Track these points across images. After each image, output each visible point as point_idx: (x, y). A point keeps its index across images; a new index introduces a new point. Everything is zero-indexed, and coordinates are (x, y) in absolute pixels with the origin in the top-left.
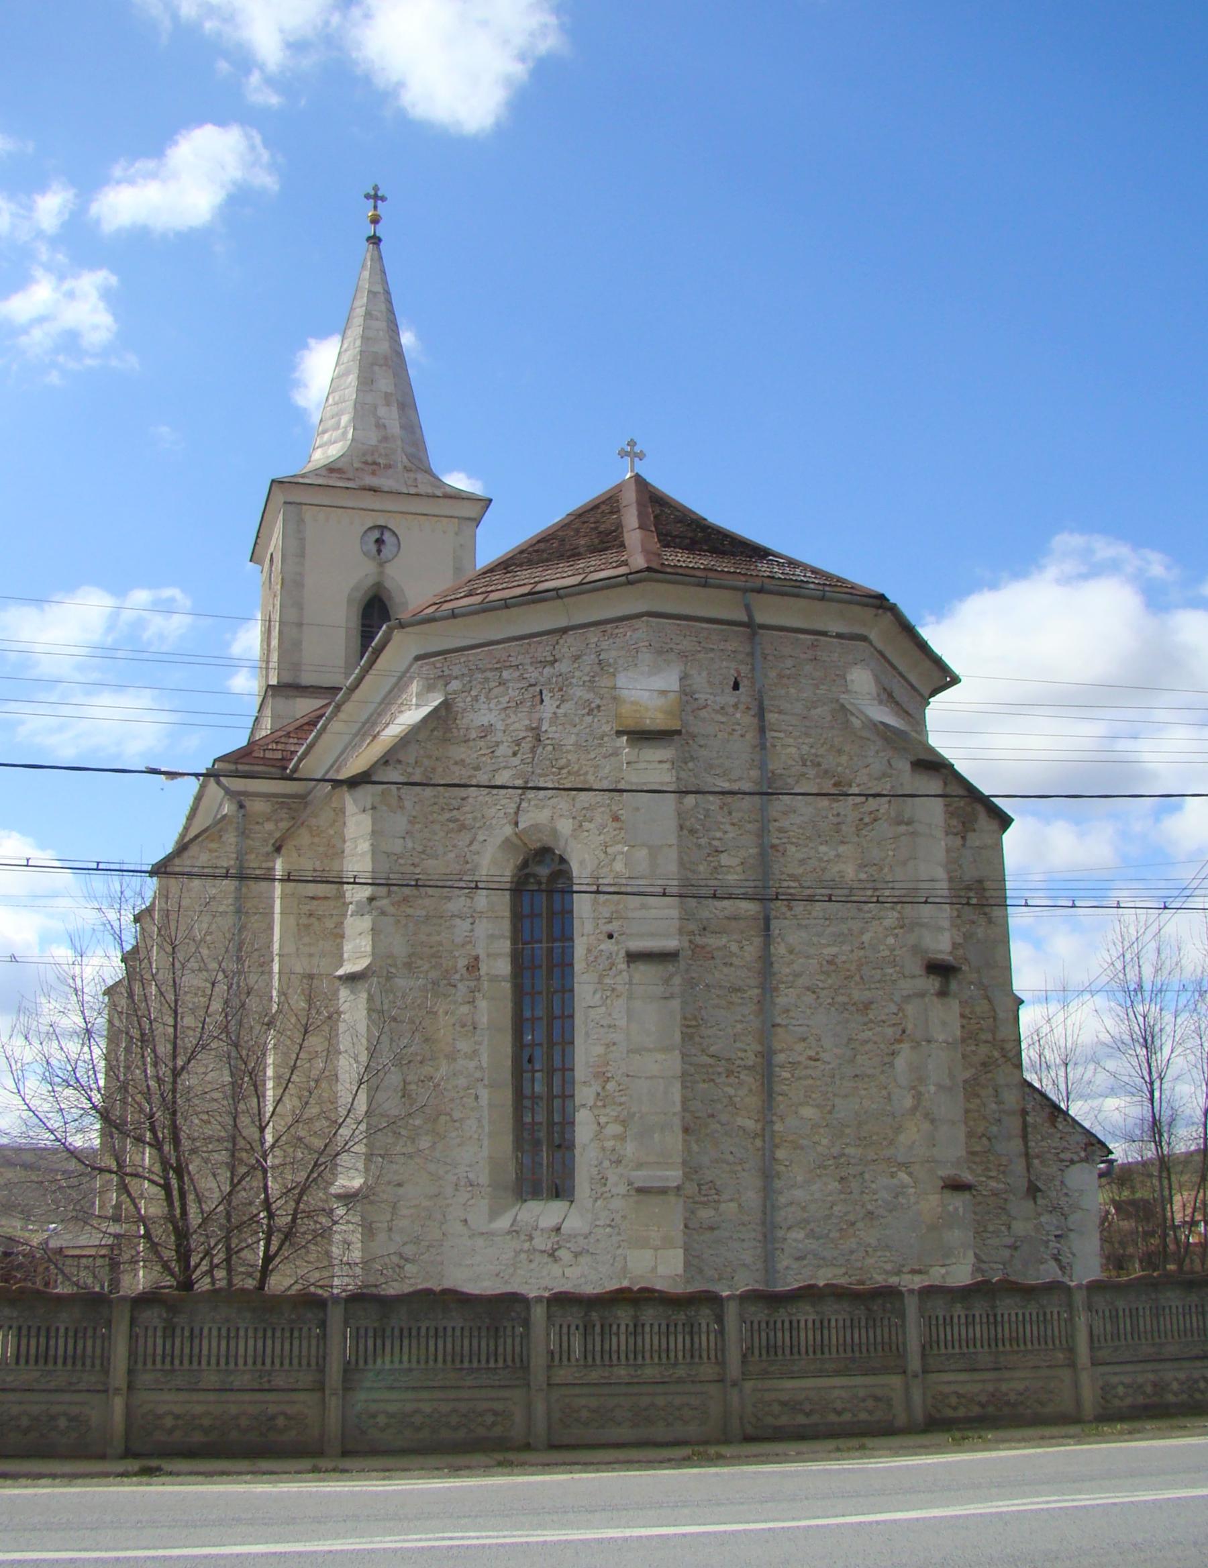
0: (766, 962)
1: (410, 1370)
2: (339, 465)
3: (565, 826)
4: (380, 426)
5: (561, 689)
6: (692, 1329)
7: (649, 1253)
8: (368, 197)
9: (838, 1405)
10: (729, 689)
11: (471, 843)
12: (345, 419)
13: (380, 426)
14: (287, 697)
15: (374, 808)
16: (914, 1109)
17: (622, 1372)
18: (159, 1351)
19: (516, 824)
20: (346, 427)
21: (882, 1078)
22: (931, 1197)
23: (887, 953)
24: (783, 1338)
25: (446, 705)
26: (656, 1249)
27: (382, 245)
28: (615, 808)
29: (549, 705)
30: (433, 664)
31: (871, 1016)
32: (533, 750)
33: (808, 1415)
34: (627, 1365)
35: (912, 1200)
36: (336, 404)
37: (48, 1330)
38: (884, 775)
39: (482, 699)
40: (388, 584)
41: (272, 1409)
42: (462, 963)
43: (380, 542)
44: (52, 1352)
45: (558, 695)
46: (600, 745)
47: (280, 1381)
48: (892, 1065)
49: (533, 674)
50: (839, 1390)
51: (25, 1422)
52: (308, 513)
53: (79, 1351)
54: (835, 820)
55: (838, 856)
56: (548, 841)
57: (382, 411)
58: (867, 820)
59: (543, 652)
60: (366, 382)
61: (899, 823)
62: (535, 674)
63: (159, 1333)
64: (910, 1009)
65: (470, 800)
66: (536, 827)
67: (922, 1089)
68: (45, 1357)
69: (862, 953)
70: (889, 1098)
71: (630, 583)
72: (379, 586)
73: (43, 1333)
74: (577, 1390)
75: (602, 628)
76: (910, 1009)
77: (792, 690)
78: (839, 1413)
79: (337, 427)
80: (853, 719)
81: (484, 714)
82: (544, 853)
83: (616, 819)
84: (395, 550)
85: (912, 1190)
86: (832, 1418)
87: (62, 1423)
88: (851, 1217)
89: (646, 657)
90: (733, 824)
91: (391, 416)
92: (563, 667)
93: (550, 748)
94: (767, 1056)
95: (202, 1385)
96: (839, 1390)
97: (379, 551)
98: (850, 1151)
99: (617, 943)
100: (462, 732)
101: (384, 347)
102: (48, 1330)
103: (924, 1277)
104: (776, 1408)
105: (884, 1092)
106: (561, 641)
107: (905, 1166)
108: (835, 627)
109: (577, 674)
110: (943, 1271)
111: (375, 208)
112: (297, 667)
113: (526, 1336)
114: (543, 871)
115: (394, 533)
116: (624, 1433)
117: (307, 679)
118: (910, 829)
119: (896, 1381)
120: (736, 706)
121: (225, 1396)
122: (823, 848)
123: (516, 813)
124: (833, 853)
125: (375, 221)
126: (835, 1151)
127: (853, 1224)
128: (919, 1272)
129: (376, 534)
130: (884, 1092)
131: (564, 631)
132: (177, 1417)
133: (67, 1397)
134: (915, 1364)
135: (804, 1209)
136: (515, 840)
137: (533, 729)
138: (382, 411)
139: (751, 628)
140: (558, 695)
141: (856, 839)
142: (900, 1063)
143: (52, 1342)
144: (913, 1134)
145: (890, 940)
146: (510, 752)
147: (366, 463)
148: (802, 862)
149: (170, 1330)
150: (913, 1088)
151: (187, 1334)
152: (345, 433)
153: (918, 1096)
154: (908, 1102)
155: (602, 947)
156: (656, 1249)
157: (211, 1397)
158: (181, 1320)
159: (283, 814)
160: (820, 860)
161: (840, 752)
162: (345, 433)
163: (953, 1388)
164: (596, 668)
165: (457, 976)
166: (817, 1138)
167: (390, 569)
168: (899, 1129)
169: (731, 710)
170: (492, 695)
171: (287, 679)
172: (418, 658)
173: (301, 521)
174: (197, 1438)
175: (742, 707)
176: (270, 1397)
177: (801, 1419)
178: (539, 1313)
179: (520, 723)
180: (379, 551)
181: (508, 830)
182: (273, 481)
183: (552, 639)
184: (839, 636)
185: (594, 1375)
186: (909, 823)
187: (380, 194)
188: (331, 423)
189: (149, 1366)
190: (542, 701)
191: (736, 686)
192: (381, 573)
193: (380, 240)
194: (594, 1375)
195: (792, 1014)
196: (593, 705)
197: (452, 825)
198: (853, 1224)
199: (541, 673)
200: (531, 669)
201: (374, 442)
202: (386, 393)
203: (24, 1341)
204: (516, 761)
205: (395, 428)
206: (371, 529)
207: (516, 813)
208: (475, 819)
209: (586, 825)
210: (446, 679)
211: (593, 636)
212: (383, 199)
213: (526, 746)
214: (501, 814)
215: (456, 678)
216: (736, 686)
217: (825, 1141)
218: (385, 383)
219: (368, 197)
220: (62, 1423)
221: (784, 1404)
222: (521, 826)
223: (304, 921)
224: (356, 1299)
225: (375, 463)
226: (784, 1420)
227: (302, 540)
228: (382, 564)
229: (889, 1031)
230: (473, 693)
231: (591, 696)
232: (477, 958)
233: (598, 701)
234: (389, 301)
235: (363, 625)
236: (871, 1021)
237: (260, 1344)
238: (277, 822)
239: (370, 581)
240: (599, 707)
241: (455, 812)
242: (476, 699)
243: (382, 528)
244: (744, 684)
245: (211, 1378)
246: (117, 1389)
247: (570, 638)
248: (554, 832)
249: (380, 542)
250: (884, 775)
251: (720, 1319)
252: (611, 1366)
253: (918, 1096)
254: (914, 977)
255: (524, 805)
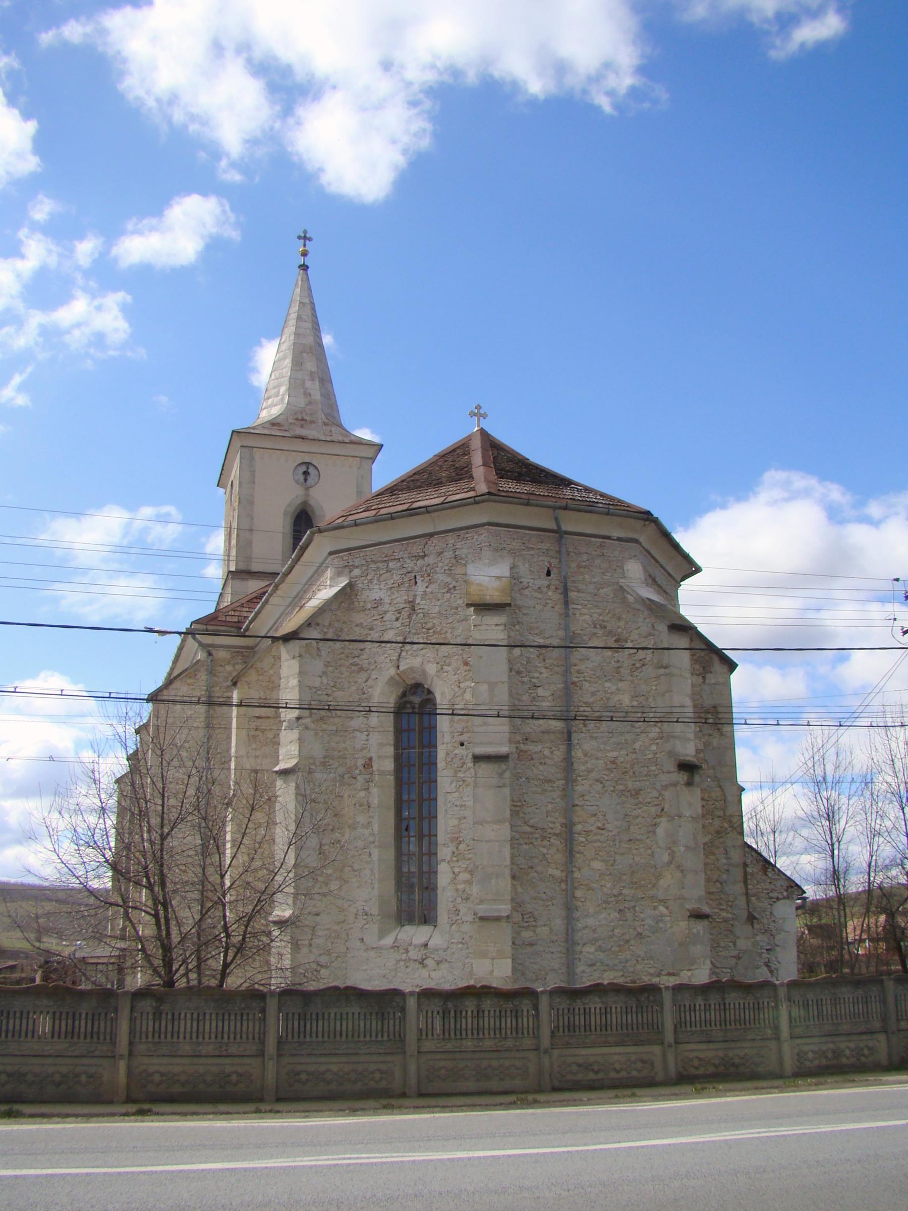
0: (568, 762)
1: (323, 1042)
2: (278, 421)
3: (431, 669)
4: (307, 394)
5: (429, 575)
6: (516, 1014)
7: (487, 962)
8: (299, 238)
9: (617, 1066)
10: (544, 575)
11: (366, 681)
12: (283, 389)
13: (307, 394)
14: (243, 579)
15: (300, 656)
16: (670, 863)
17: (469, 1044)
18: (151, 1029)
19: (398, 667)
20: (283, 395)
21: (648, 841)
22: (681, 923)
23: (651, 756)
24: (579, 1020)
25: (350, 585)
26: (493, 959)
27: (309, 270)
28: (465, 656)
29: (421, 586)
30: (342, 557)
31: (640, 799)
32: (410, 616)
33: (596, 1072)
34: (147, 1042)
35: (669, 925)
36: (277, 379)
37: (74, 1014)
38: (650, 634)
39: (375, 581)
40: (312, 502)
41: (228, 1069)
42: (360, 762)
43: (306, 473)
44: (76, 1030)
45: (427, 579)
46: (456, 614)
47: (233, 1050)
48: (654, 832)
49: (409, 564)
50: (616, 1055)
51: (57, 1078)
52: (257, 454)
53: (95, 1030)
54: (616, 665)
55: (618, 689)
56: (420, 679)
57: (308, 384)
58: (638, 665)
59: (417, 549)
60: (297, 364)
61: (659, 668)
62: (412, 565)
63: (151, 1017)
64: (666, 794)
65: (367, 651)
66: (412, 669)
67: (675, 849)
68: (71, 1033)
69: (634, 756)
70: (652, 855)
71: (476, 503)
72: (305, 503)
73: (70, 1017)
74: (438, 1056)
75: (457, 533)
76: (666, 794)
77: (587, 577)
78: (618, 1072)
79: (279, 392)
80: (628, 596)
81: (376, 593)
82: (417, 687)
83: (466, 664)
84: (316, 479)
85: (668, 919)
86: (613, 1075)
87: (83, 1078)
88: (627, 937)
89: (487, 553)
90: (546, 668)
91: (314, 388)
92: (430, 560)
93: (421, 615)
94: (569, 826)
95: (180, 1053)
96: (616, 1055)
97: (306, 480)
98: (625, 891)
99: (467, 749)
100: (362, 604)
101: (310, 340)
102: (74, 1014)
103: (677, 978)
104: (574, 1068)
105: (649, 852)
106: (429, 542)
107: (663, 901)
108: (616, 534)
109: (440, 565)
110: (689, 973)
111: (305, 245)
112: (249, 559)
113: (403, 1019)
114: (416, 700)
115: (316, 468)
116: (471, 1085)
117: (255, 567)
118: (667, 671)
119: (657, 1049)
120: (548, 587)
121: (195, 1060)
122: (608, 684)
123: (398, 660)
124: (614, 688)
125: (304, 254)
126: (615, 892)
127: (628, 941)
128: (673, 974)
129: (304, 468)
130: (649, 852)
131: (431, 535)
132: (162, 1075)
133: (86, 1061)
134: (669, 1037)
135: (594, 931)
136: (397, 678)
137: (410, 602)
138: (308, 384)
139: (559, 533)
140: (427, 579)
141: (630, 678)
142: (660, 831)
143: (77, 1023)
144: (668, 880)
145: (654, 747)
146: (394, 618)
147: (297, 419)
148: (593, 694)
149: (158, 1015)
150: (670, 849)
151: (170, 1017)
152: (283, 399)
153: (672, 854)
154: (666, 858)
155: (456, 751)
156: (493, 959)
157: (186, 1061)
158: (165, 1007)
159: (239, 659)
160: (606, 692)
161: (619, 619)
162: (283, 399)
163: (696, 1054)
164: (454, 561)
165: (357, 772)
166: (603, 883)
167: (312, 492)
168: (658, 877)
169: (545, 590)
170: (381, 579)
171: (242, 567)
172: (331, 553)
173: (252, 459)
174: (177, 1089)
175: (553, 587)
176: (227, 1061)
177: (592, 1076)
178: (412, 1003)
179: (401, 598)
180: (306, 480)
181: (392, 672)
182: (233, 431)
183: (424, 540)
184: (619, 539)
185: (449, 1046)
186: (666, 668)
187: (308, 236)
188: (273, 392)
189: (144, 1039)
190: (416, 583)
191: (549, 574)
192: (307, 495)
193: (307, 267)
194: (449, 1046)
195: (586, 798)
196: (451, 586)
197: (353, 668)
198: (628, 941)
199: (416, 564)
200: (409, 561)
201: (303, 405)
202: (312, 373)
203: (57, 1022)
204: (398, 624)
205: (317, 396)
206: (300, 464)
207: (398, 660)
208: (369, 664)
209: (446, 668)
210: (350, 568)
211: (451, 539)
212: (310, 239)
213: (405, 614)
214: (388, 660)
215: (357, 567)
216: (549, 574)
217: (609, 885)
218: (310, 365)
219: (299, 238)
220: (83, 1078)
221: (579, 1065)
222: (401, 668)
223: (252, 733)
224: (286, 993)
225: (303, 420)
226: (579, 1077)
227: (253, 473)
228: (307, 489)
229: (653, 810)
230: (369, 577)
231: (449, 580)
232: (371, 759)
233: (454, 583)
234: (314, 309)
235: (294, 531)
236: (640, 803)
237: (220, 1024)
238: (234, 665)
239: (299, 501)
240: (455, 587)
241: (356, 659)
242: (371, 581)
243: (308, 464)
244: (554, 572)
245: (186, 1048)
246: (122, 1055)
247: (435, 540)
248: (424, 673)
249: (306, 473)
250: (650, 634)
251: (536, 1008)
252: (461, 1039)
253: (672, 854)
254: (669, 772)
255: (403, 654)
